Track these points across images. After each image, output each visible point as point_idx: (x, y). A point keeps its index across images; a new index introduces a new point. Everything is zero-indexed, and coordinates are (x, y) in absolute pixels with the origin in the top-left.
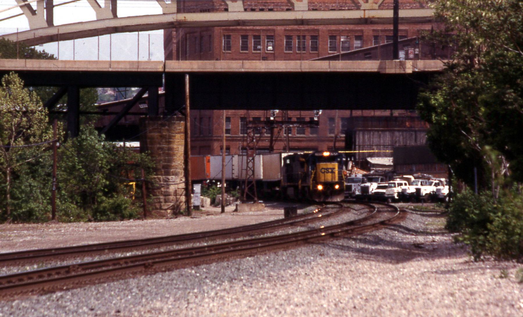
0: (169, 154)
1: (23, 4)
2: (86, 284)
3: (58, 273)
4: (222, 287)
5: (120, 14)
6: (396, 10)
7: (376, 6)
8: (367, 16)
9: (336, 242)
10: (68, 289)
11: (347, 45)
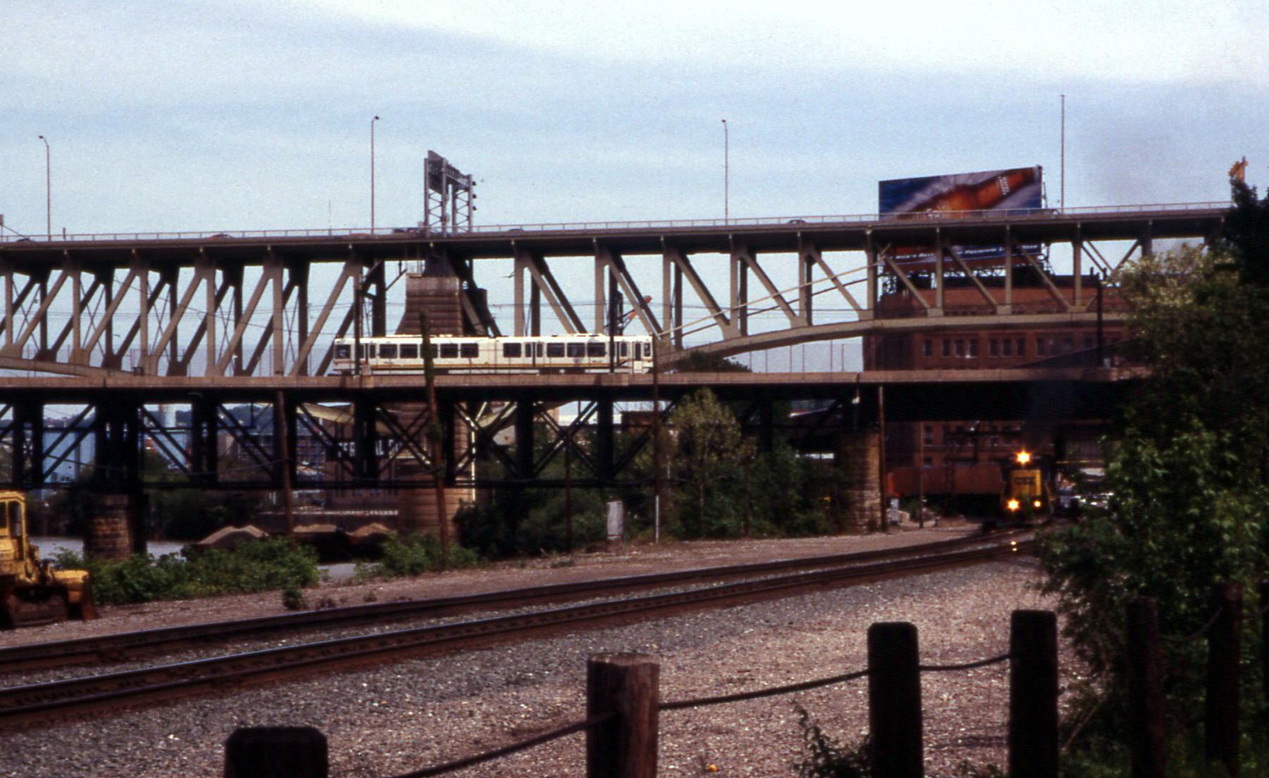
0: (864, 467)
5: (815, 321)
7: (1084, 308)
8: (1074, 319)
10: (748, 604)
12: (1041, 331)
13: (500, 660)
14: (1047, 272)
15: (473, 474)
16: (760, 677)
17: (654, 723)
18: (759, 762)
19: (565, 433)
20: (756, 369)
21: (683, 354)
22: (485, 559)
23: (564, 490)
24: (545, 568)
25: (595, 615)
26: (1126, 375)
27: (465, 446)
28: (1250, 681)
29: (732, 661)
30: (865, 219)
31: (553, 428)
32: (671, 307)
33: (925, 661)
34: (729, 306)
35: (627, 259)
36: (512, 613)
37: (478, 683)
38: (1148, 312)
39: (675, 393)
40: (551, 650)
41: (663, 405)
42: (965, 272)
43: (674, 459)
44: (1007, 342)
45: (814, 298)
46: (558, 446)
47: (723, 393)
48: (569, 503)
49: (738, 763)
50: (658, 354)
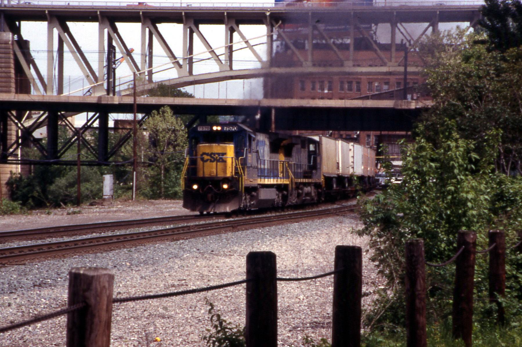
1: (174, 61)
2: (198, 236)
3: (183, 230)
4: (275, 239)
5: (234, 68)
6: (406, 67)
7: (397, 64)
8: (390, 71)
9: (353, 215)
10: (187, 239)
11: (378, 88)
12: (371, 77)
13: (30, 271)
14: (375, 42)
15: (19, 156)
16: (191, 284)
17: (109, 310)
18: (186, 336)
19: (78, 132)
20: (197, 96)
21: (153, 85)
22: (25, 208)
23: (76, 167)
24: (62, 214)
25: (92, 244)
26: (420, 105)
27: (14, 138)
28: (480, 291)
29: (175, 274)
30: (266, 6)
31: (71, 129)
32: (146, 56)
33: (279, 276)
34: (182, 57)
35: (118, 25)
36: (40, 242)
37: (15, 286)
38: (434, 67)
39: (147, 109)
40: (62, 265)
41: (140, 116)
42: (326, 40)
43: (145, 151)
44: (350, 83)
45: (234, 53)
46: (73, 139)
47: (177, 110)
48: (79, 175)
49: (173, 336)
50: (137, 84)
